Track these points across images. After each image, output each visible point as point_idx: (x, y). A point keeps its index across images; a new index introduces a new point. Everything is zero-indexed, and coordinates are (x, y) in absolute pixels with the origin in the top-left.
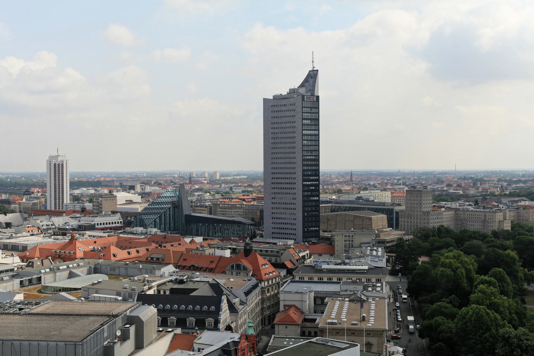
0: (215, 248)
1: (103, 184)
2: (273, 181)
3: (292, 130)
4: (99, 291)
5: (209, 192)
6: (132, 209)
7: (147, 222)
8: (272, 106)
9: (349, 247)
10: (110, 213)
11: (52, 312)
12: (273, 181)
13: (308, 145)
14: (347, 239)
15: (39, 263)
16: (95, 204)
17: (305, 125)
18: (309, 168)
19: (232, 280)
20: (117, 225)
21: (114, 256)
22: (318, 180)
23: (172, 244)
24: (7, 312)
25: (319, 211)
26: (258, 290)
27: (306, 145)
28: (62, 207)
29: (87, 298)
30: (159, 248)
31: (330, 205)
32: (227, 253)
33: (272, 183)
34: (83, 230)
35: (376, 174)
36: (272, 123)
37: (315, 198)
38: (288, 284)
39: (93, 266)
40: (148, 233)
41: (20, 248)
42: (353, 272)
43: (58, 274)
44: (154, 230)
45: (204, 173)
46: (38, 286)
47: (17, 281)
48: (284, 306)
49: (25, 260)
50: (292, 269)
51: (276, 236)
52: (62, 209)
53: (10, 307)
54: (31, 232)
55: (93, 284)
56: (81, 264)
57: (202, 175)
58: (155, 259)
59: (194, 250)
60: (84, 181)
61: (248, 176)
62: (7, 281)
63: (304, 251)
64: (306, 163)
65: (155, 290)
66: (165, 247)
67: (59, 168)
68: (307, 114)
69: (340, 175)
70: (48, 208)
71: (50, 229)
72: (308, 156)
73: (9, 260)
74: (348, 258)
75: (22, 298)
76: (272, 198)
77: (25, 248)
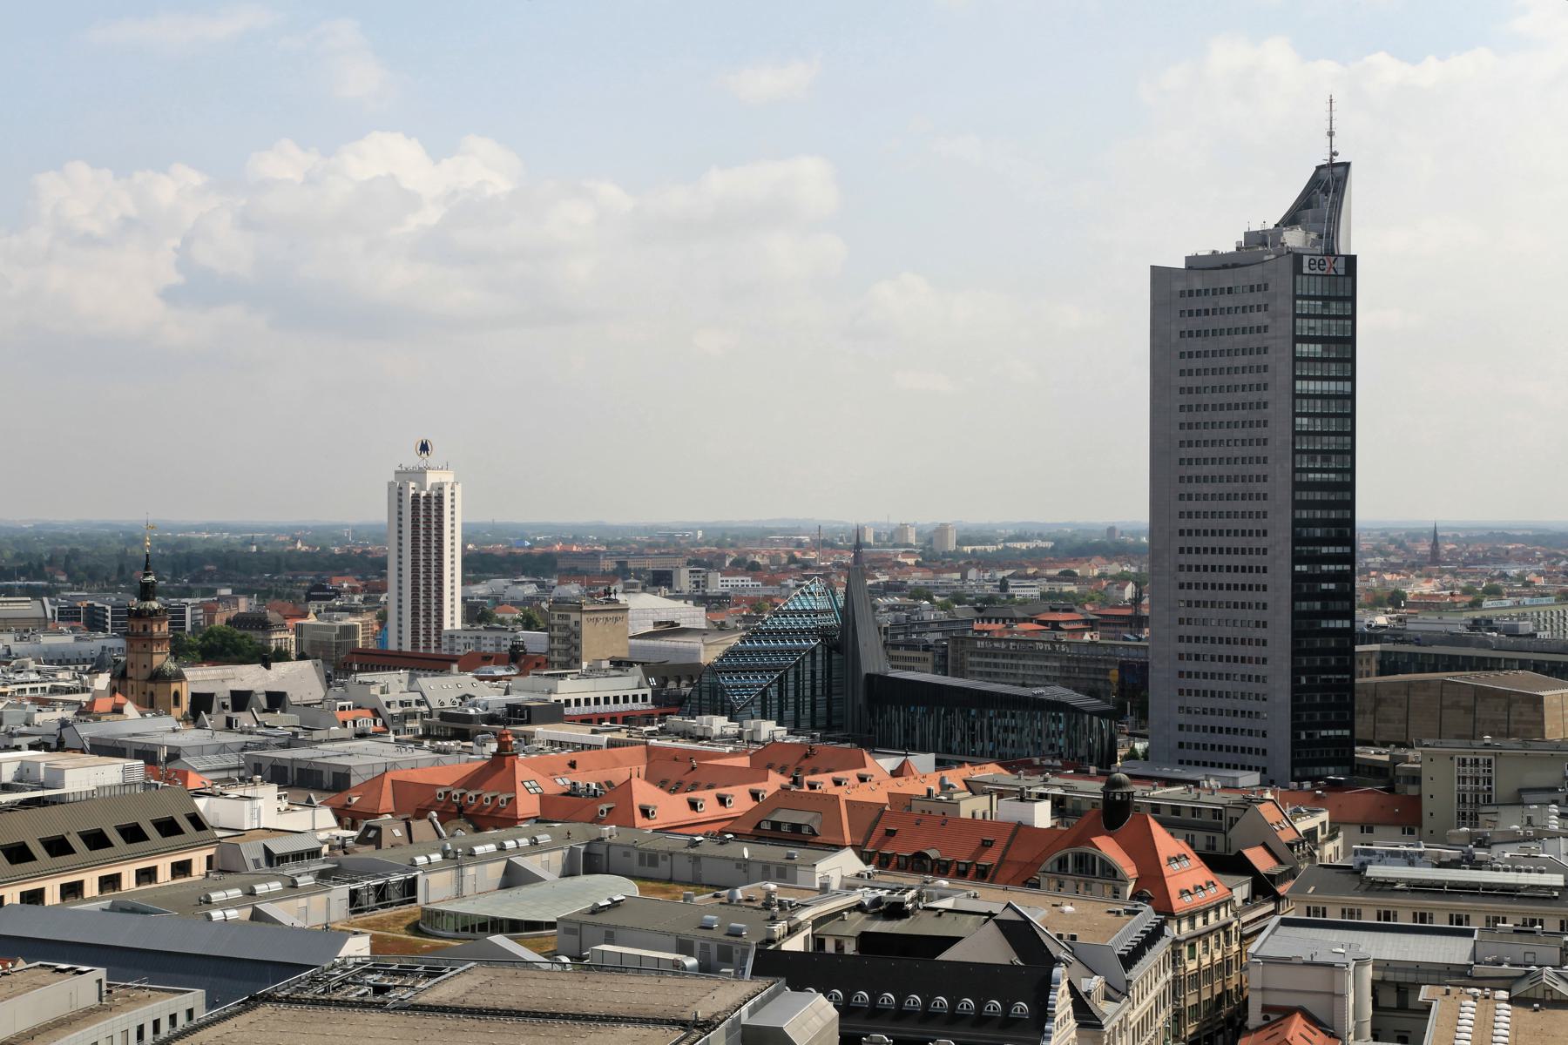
0: (990, 793)
1: (561, 564)
2: (1185, 559)
3: (1254, 378)
4: (618, 934)
5: (929, 598)
6: (676, 650)
7: (736, 699)
8: (1182, 293)
9: (1472, 808)
10: (606, 664)
11: (490, 1005)
12: (1185, 559)
13: (1315, 433)
14: (1469, 771)
15: (397, 833)
16: (556, 633)
17: (1302, 359)
18: (1318, 514)
19: (1068, 909)
20: (631, 706)
21: (645, 812)
22: (1350, 559)
23: (838, 775)
24: (337, 996)
25: (1351, 670)
26: (1161, 949)
27: (1308, 433)
28: (438, 642)
29: (577, 958)
30: (793, 789)
31: (1376, 647)
32: (1042, 816)
33: (1181, 568)
34: (522, 723)
35: (1524, 539)
36: (1182, 355)
37: (1339, 624)
38: (1273, 932)
39: (582, 848)
40: (746, 738)
41: (325, 778)
42: (1508, 892)
43: (470, 871)
44: (768, 728)
45: (902, 529)
46: (405, 909)
47: (341, 892)
48: (1266, 1009)
49: (348, 821)
50: (1272, 877)
51: (1192, 754)
52: (439, 646)
53: (344, 982)
54: (350, 724)
55: (596, 910)
56: (544, 838)
57: (896, 537)
58: (784, 829)
59: (922, 799)
60: (499, 553)
61: (1058, 541)
62: (309, 891)
63: (1312, 812)
64: (1304, 496)
65: (806, 938)
66: (812, 786)
67: (428, 509)
68: (1312, 323)
69: (1392, 541)
71: (413, 716)
72: (1315, 471)
73: (300, 819)
74: (1480, 845)
75: (367, 952)
76: (1181, 621)
77: (341, 781)
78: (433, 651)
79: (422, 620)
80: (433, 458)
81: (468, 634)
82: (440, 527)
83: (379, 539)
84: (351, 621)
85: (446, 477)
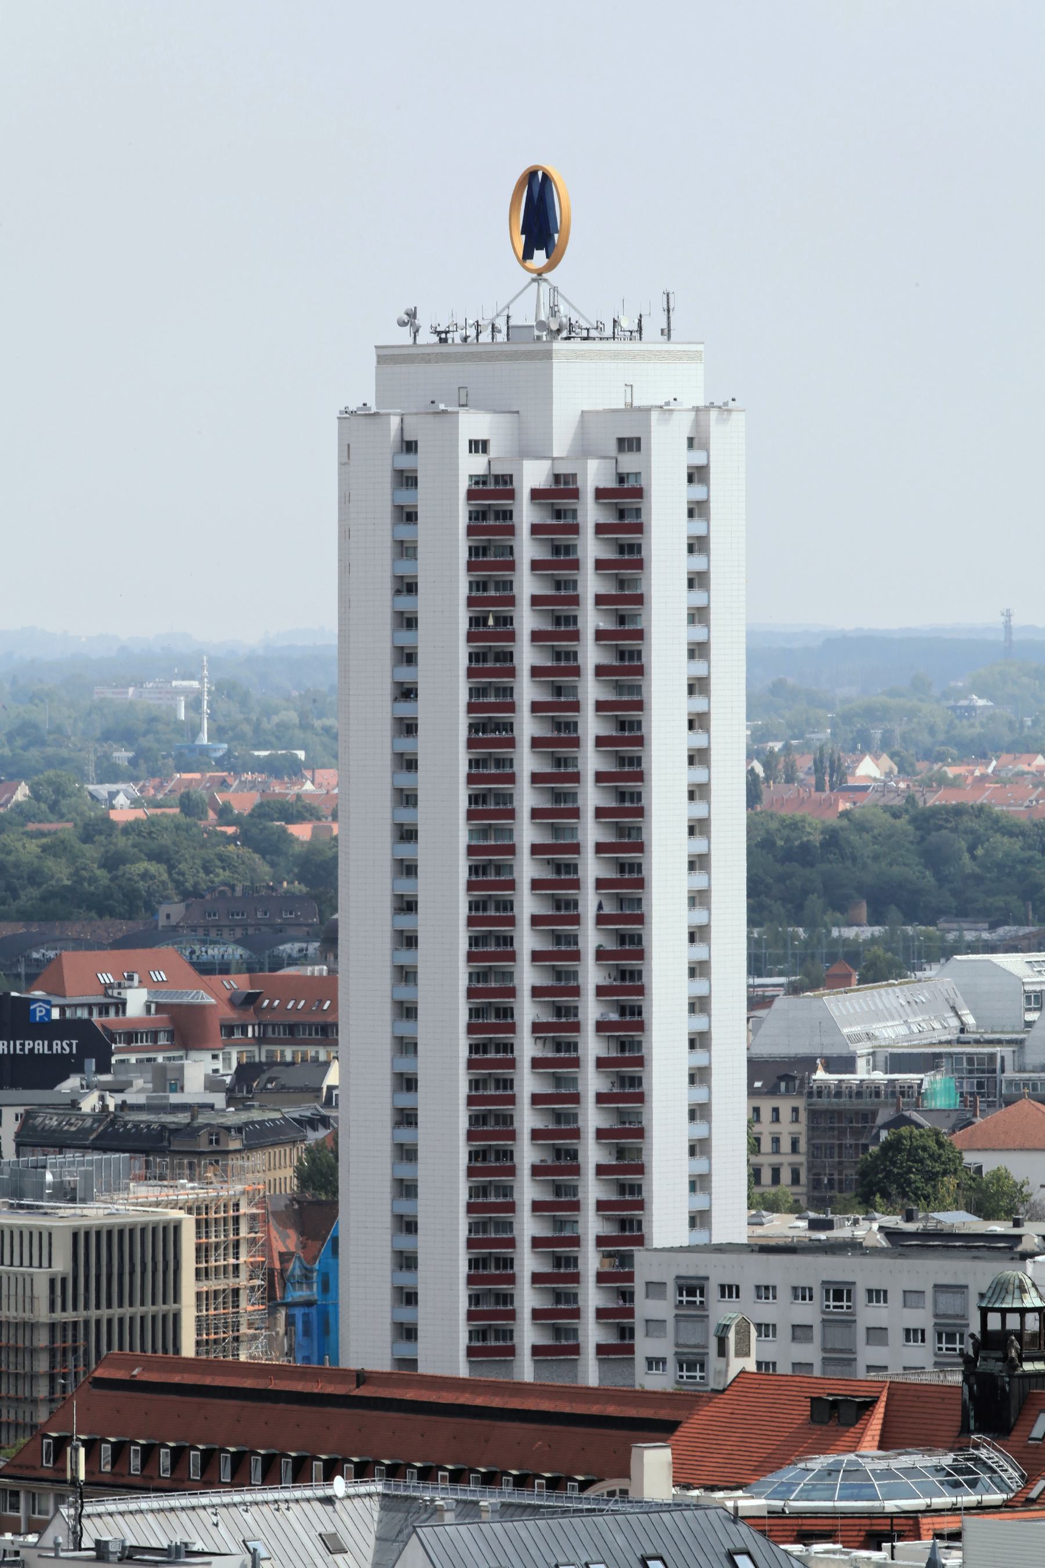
28: (619, 1317)
52: (618, 1350)
67: (559, 561)
70: (365, 1344)
78: (591, 1373)
79: (527, 1191)
80: (586, 276)
81: (780, 1271)
82: (627, 664)
83: (256, 718)
84: (136, 1200)
85: (665, 383)
